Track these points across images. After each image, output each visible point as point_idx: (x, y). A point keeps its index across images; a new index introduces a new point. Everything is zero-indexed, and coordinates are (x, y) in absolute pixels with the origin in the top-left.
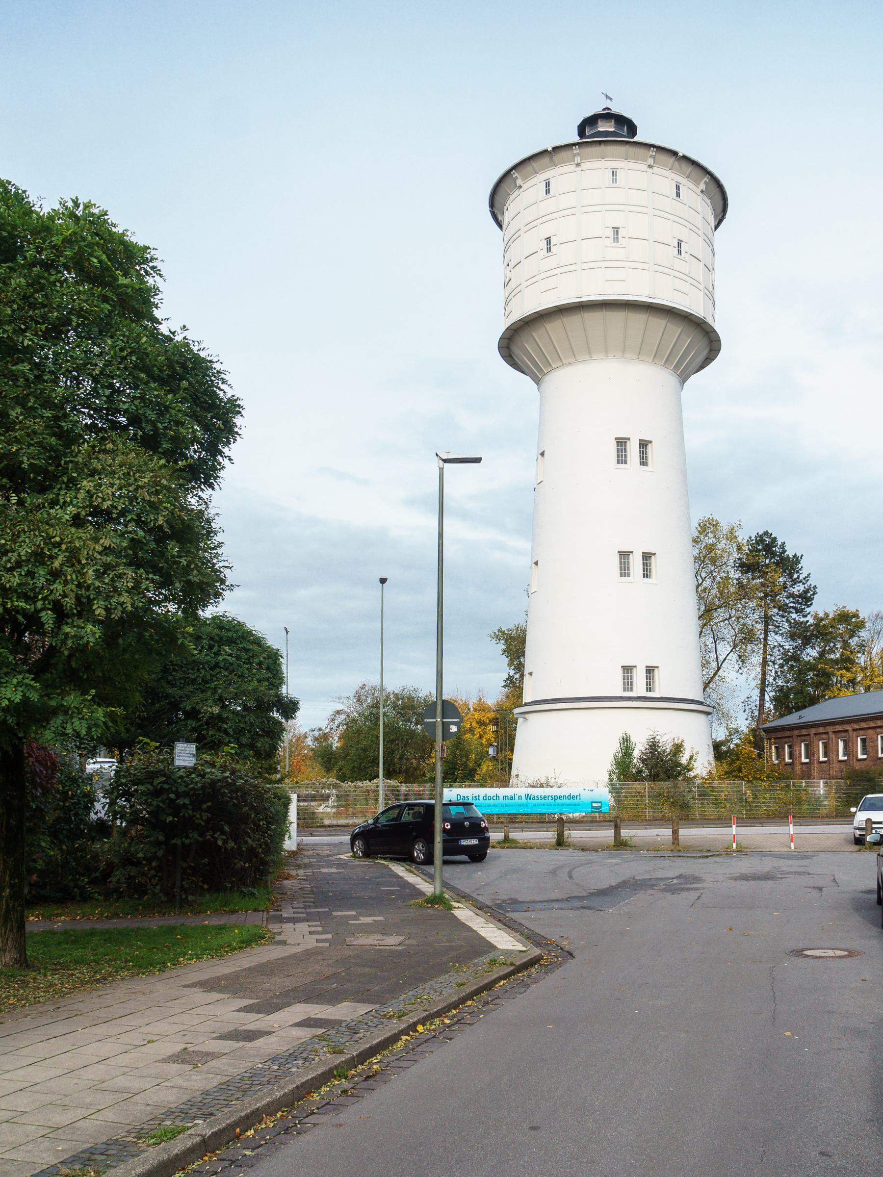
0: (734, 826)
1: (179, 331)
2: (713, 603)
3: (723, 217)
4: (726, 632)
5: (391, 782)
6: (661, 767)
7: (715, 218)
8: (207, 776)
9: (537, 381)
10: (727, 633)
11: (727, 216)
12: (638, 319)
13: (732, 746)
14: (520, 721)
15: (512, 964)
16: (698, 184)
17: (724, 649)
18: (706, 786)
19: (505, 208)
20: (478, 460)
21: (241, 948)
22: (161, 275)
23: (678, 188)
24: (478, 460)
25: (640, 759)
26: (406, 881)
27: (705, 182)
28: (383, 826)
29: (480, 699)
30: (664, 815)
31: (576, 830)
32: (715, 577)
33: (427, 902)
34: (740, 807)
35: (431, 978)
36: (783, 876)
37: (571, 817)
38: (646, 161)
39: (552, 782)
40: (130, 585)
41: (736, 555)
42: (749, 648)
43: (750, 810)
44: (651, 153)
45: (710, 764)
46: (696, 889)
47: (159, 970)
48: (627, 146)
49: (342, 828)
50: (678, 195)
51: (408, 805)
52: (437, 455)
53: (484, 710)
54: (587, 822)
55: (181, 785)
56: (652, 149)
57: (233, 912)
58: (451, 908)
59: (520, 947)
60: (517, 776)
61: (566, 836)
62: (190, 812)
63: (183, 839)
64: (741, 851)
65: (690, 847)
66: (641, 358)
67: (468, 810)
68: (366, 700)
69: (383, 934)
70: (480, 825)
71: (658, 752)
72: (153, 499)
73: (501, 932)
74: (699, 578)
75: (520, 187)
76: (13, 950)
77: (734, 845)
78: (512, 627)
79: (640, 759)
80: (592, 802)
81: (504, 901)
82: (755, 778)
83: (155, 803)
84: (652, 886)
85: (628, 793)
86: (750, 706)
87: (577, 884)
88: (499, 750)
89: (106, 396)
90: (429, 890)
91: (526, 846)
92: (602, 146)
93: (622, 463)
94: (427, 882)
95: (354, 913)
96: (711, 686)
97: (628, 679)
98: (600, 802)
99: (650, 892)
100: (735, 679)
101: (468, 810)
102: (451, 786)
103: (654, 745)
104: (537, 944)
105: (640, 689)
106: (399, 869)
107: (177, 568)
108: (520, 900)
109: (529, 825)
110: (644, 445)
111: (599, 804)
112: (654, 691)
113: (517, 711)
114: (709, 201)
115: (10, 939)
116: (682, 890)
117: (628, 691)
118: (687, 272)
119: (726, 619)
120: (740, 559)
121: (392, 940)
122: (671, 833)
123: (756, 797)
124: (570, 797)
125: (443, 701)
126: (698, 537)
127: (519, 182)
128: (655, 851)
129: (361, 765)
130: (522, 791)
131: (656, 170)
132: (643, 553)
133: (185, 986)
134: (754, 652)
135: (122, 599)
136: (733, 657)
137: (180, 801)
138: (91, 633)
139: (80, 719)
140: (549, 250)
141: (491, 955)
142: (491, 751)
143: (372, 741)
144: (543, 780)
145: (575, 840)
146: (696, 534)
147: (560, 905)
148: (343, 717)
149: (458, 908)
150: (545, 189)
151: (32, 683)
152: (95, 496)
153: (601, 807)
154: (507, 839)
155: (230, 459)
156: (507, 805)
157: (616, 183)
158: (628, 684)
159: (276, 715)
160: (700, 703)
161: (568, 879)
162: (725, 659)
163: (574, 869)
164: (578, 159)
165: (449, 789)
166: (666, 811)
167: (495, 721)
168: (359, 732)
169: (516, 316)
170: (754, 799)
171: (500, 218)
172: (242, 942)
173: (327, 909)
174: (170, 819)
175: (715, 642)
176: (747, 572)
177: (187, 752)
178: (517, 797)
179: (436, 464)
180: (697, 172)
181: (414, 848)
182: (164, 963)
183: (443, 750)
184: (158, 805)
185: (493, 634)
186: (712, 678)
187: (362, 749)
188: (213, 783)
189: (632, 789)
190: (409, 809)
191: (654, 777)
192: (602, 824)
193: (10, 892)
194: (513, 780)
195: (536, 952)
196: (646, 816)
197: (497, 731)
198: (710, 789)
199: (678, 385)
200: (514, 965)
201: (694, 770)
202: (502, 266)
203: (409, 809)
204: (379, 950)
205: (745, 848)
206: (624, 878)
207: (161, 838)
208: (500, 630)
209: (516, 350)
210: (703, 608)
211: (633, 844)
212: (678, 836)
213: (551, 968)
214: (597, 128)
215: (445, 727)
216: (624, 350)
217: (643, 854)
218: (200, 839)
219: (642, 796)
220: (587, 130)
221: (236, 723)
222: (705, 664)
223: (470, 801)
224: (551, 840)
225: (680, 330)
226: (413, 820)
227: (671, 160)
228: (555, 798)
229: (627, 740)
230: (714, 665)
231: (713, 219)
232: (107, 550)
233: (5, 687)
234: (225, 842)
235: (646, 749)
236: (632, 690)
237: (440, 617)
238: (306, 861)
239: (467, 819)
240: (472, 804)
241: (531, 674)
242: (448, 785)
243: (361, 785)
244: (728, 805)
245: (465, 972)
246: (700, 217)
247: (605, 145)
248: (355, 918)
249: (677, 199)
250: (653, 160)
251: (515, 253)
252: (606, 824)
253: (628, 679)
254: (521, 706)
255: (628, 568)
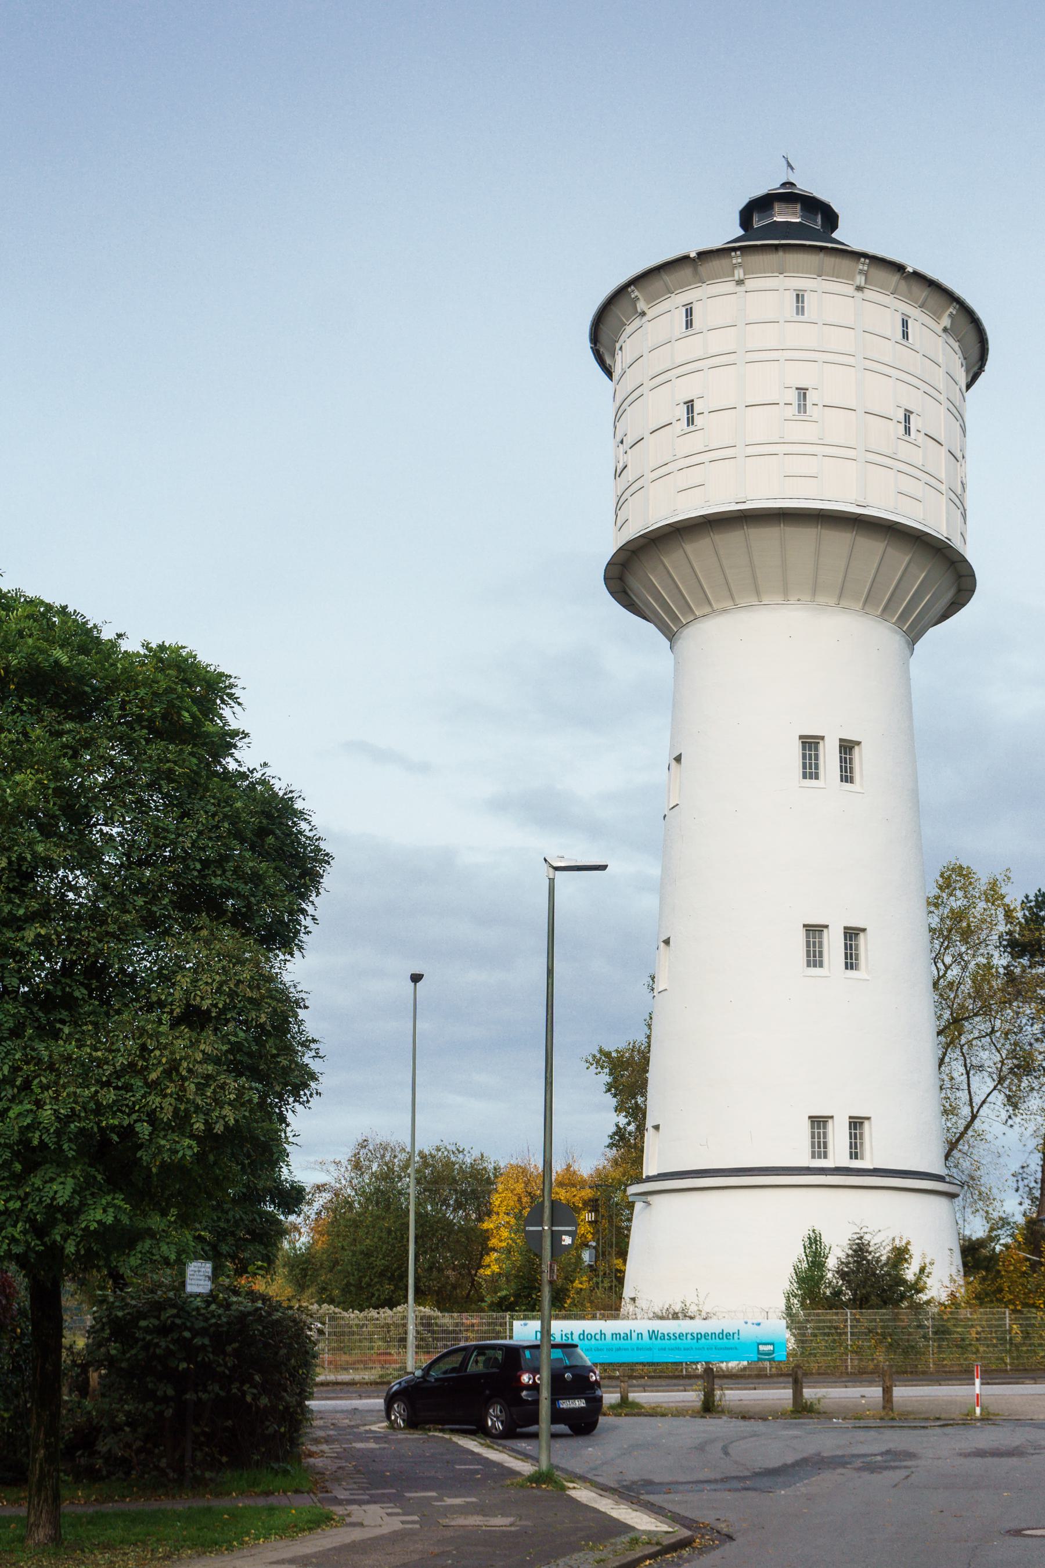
0: (978, 1381)
1: (258, 768)
2: (962, 1007)
3: (981, 369)
4: (984, 1055)
5: (426, 1310)
6: (872, 1286)
7: (967, 371)
8: (234, 1307)
9: (671, 636)
10: (988, 1057)
11: (986, 368)
12: (839, 540)
13: (998, 1248)
14: (639, 1206)
15: (658, 1544)
16: (939, 318)
17: (982, 1085)
18: (945, 1317)
19: (618, 346)
20: (603, 868)
21: (310, 1529)
22: (239, 704)
23: (905, 324)
24: (603, 868)
25: (838, 1272)
26: (487, 1459)
27: (951, 315)
28: (437, 1380)
29: (569, 1166)
30: (877, 1366)
31: (732, 1389)
32: (967, 963)
33: (531, 1482)
34: (1001, 1351)
35: (564, 1555)
36: (1038, 1451)
37: (724, 1369)
38: (853, 279)
39: (692, 1310)
40: (233, 1097)
41: (1002, 928)
42: (1024, 1084)
43: (1018, 1358)
44: (861, 267)
45: (952, 1280)
46: (906, 1467)
47: (227, 1550)
48: (822, 255)
49: (344, 1387)
50: (905, 335)
51: (477, 1347)
52: (545, 860)
53: (574, 1185)
54: (750, 1376)
55: (197, 1319)
56: (862, 260)
57: (268, 1494)
58: (564, 1488)
59: (665, 1528)
60: (633, 1299)
61: (717, 1398)
62: (211, 1356)
63: (200, 1394)
64: (987, 1418)
65: (909, 1413)
66: (843, 603)
67: (569, 1356)
68: (369, 1167)
69: (484, 1515)
70: (588, 1378)
71: (868, 1261)
72: (255, 995)
73: (638, 1514)
74: (940, 965)
75: (643, 314)
76: (47, 1525)
77: (978, 1410)
78: (622, 1045)
79: (838, 1272)
80: (759, 1344)
81: (633, 1483)
82: (1025, 1305)
83: (163, 1344)
84: (843, 1465)
85: (818, 1328)
86: (1026, 1182)
87: (736, 1462)
88: (600, 1254)
89: (197, 870)
90: (525, 1468)
91: (655, 1412)
92: (781, 254)
93: (811, 778)
94: (518, 1459)
95: (434, 1494)
96: (960, 1147)
97: (819, 1138)
98: (772, 1344)
99: (840, 1470)
100: (1000, 1136)
101: (569, 1356)
102: (526, 1318)
103: (861, 1250)
104: (689, 1528)
105: (838, 1155)
106: (471, 1444)
107: (275, 1068)
108: (657, 1480)
109: (655, 1382)
110: (847, 747)
111: (771, 1348)
112: (862, 1158)
113: (632, 1189)
114: (956, 345)
115: (44, 1511)
116: (886, 1468)
117: (819, 1157)
118: (919, 464)
119: (987, 1035)
120: (1010, 933)
121: (500, 1522)
122: (881, 1394)
123: (1027, 1335)
124: (723, 1335)
125: (553, 1203)
126: (937, 897)
127: (641, 305)
128: (855, 1416)
129: (361, 1282)
130: (643, 1326)
131: (869, 294)
132: (845, 928)
133: (271, 1563)
134: (1033, 1089)
135: (224, 1112)
136: (998, 1098)
137: (198, 1341)
138: (187, 1147)
139: (168, 1243)
140: (690, 421)
141: (632, 1535)
142: (586, 1256)
143: (380, 1238)
144: (677, 1308)
145: (732, 1403)
146: (936, 891)
147: (713, 1486)
148: (327, 1196)
149: (574, 1488)
150: (684, 319)
151: (122, 1204)
152: (193, 995)
153: (773, 1352)
154: (624, 1402)
155: (314, 919)
156: (619, 1349)
157: (803, 314)
158: (820, 1147)
159: (270, 1208)
160: (939, 1178)
161: (723, 1456)
162: (984, 1102)
163: (732, 1442)
164: (739, 274)
165: (522, 1322)
166: (881, 1359)
167: (593, 1205)
168: (356, 1224)
169: (634, 530)
170: (1024, 1338)
171: (608, 361)
172: (310, 1521)
173: (394, 1491)
174: (183, 1365)
175: (968, 1073)
176: (1021, 956)
177: (202, 1273)
178: (634, 1335)
179: (545, 871)
180: (935, 299)
181: (487, 1413)
182: (230, 1542)
183: (552, 1270)
184: (167, 1347)
185: (590, 1059)
186: (962, 1134)
187: (362, 1252)
188: (244, 1315)
189: (824, 1321)
190: (478, 1355)
191: (861, 1302)
192: (775, 1379)
193: (45, 1454)
194: (627, 1307)
195: (686, 1533)
196: (847, 1367)
197: (596, 1222)
198: (952, 1322)
199: (907, 652)
200: (661, 1544)
201: (927, 1291)
202: (611, 443)
203: (478, 1355)
204: (486, 1531)
205: (994, 1415)
206: (805, 1455)
207: (170, 1392)
208: (601, 1051)
209: (634, 584)
210: (947, 1015)
211: (822, 1410)
212: (891, 1396)
213: (703, 1550)
214: (773, 216)
215: (556, 1237)
216: (815, 590)
217: (836, 1423)
218: (222, 1393)
219: (840, 1334)
220: (755, 218)
221: (214, 1221)
222: (949, 1111)
223: (576, 1341)
224: (696, 1403)
225: (907, 559)
226: (486, 1371)
227: (894, 278)
228: (698, 1337)
229: (816, 1241)
230: (966, 1111)
231: (964, 374)
232: (207, 1058)
233: (94, 1209)
234: (255, 1398)
235: (848, 1256)
236: (825, 1157)
237: (549, 1085)
238: (321, 1433)
239: (568, 1368)
240: (576, 1346)
241: (657, 1128)
242: (521, 1314)
243: (377, 1316)
244: (981, 1349)
245: (602, 1551)
246: (941, 373)
247: (784, 251)
248: (436, 1499)
249: (904, 342)
250: (863, 278)
251: (634, 423)
252: (781, 1379)
253: (819, 1138)
254: (639, 1180)
255: (821, 953)
